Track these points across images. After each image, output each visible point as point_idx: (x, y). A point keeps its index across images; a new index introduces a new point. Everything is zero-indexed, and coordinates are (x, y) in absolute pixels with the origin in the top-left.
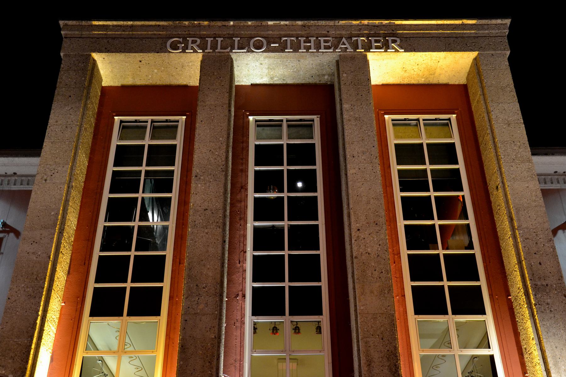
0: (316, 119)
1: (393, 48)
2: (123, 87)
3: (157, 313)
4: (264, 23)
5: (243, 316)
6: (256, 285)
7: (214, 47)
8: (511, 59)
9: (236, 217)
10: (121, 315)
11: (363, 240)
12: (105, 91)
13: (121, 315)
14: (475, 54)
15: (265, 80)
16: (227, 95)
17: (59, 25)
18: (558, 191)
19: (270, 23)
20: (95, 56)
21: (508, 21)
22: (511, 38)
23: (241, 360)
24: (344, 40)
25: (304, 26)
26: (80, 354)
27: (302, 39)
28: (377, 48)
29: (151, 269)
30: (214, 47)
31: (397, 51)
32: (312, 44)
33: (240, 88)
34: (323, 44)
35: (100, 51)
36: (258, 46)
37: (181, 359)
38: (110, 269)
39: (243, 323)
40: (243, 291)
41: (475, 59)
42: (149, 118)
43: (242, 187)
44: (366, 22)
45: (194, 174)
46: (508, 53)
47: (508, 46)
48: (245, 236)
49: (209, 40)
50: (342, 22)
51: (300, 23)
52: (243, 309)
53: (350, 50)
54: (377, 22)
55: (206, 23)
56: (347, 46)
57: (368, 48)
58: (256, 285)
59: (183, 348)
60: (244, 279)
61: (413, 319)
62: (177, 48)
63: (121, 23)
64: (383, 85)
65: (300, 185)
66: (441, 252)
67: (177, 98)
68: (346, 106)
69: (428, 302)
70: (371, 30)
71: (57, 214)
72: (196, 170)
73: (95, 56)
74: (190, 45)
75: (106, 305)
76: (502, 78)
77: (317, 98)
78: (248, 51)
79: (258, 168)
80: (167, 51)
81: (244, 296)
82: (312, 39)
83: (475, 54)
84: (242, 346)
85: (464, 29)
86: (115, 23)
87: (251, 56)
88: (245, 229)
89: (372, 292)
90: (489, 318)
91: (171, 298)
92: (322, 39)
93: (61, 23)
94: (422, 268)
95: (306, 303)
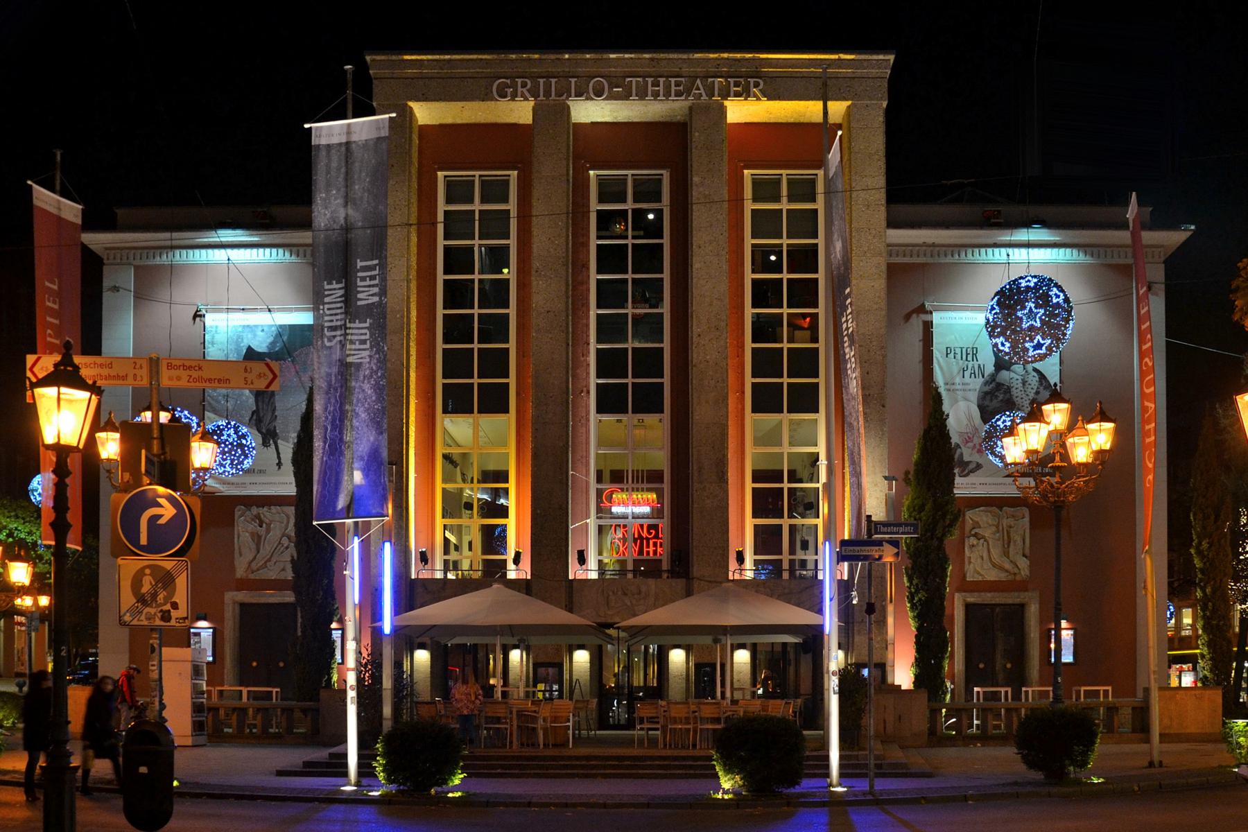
0: (666, 174)
1: (755, 96)
2: (442, 126)
3: (507, 411)
4: (605, 56)
5: (588, 413)
6: (600, 381)
7: (547, 93)
8: (888, 112)
9: (578, 305)
10: (472, 412)
11: (704, 349)
12: (423, 128)
13: (472, 412)
14: (849, 103)
15: (608, 119)
16: (564, 162)
17: (365, 62)
18: (924, 265)
19: (612, 56)
20: (411, 104)
21: (892, 58)
22: (893, 81)
23: (587, 456)
24: (698, 81)
25: (652, 59)
26: (440, 451)
27: (650, 80)
28: (737, 95)
29: (496, 363)
30: (547, 93)
31: (758, 99)
32: (661, 88)
33: (579, 127)
34: (673, 88)
35: (418, 100)
36: (598, 93)
37: (534, 466)
38: (456, 364)
39: (588, 420)
40: (587, 386)
41: (849, 107)
42: (477, 173)
43: (583, 266)
44: (725, 55)
45: (534, 267)
46: (885, 104)
47: (886, 95)
48: (588, 326)
49: (542, 81)
50: (697, 56)
51: (647, 56)
52: (587, 406)
53: (704, 97)
54: (739, 56)
55: (536, 56)
56: (702, 91)
57: (726, 96)
58: (600, 381)
59: (535, 456)
60: (588, 374)
61: (749, 416)
62: (505, 97)
63: (437, 57)
64: (746, 124)
65: (651, 216)
66: (785, 345)
67: (507, 145)
68: (696, 179)
69: (766, 401)
70: (731, 67)
71: (402, 317)
72: (536, 264)
73: (411, 104)
74: (520, 89)
75: (458, 402)
76: (875, 142)
77: (668, 144)
78: (587, 99)
79: (600, 277)
80: (493, 99)
81: (588, 392)
82: (662, 80)
83: (849, 103)
84: (588, 443)
85: (840, 67)
86: (430, 57)
87: (590, 103)
88: (588, 283)
89: (707, 402)
90: (821, 417)
91: (518, 394)
92: (673, 80)
93: (368, 58)
94: (765, 363)
95: (648, 401)
